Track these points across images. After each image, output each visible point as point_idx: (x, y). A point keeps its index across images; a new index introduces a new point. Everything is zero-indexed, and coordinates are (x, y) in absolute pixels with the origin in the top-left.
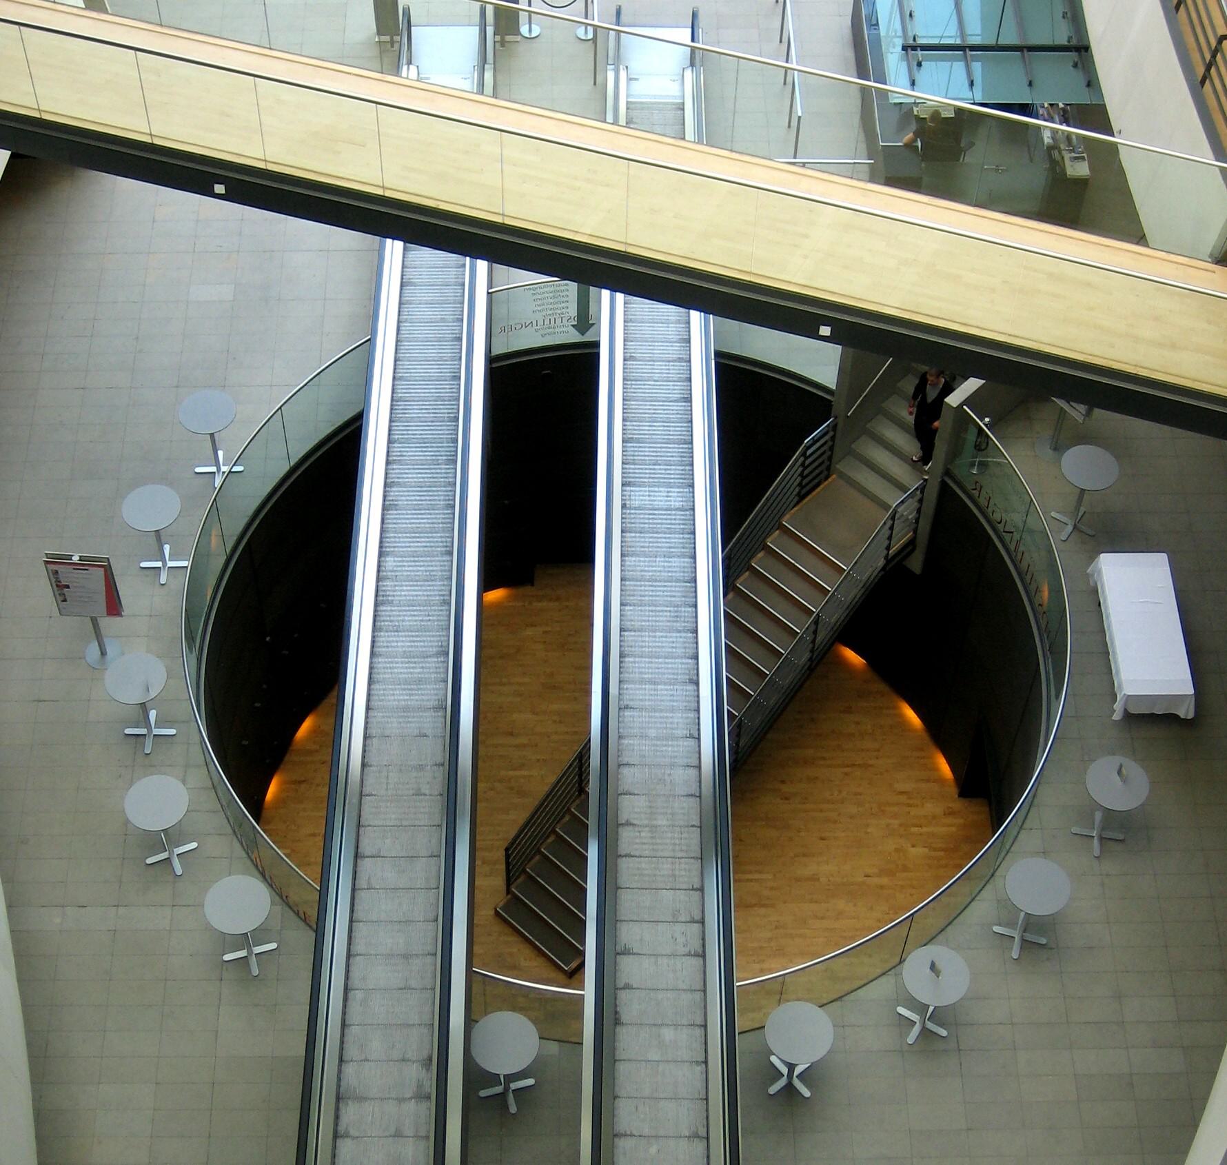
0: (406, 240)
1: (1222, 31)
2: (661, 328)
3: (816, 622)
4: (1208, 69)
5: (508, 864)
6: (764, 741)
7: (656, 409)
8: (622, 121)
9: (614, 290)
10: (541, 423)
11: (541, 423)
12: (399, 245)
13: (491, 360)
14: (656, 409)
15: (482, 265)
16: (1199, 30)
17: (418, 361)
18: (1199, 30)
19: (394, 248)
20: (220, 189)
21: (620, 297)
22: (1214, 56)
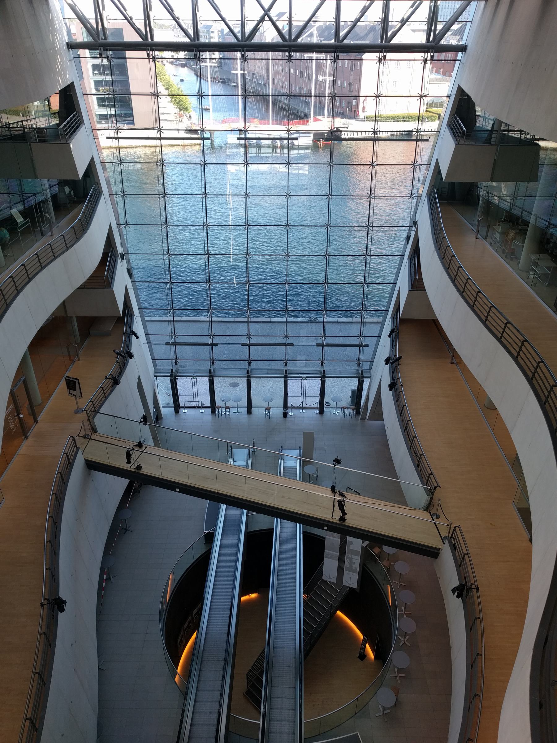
0: (227, 504)
1: (552, 383)
2: (450, 6)
3: (331, 606)
4: (461, 562)
5: (247, 679)
6: (319, 634)
7: (290, 545)
8: (282, 475)
9: (277, 518)
10: (258, 547)
11: (258, 547)
12: (225, 505)
13: (248, 535)
14: (290, 545)
15: (245, 511)
16: (543, 378)
17: (230, 530)
18: (543, 378)
19: (223, 507)
20: (178, 490)
21: (279, 520)
22: (428, 479)
